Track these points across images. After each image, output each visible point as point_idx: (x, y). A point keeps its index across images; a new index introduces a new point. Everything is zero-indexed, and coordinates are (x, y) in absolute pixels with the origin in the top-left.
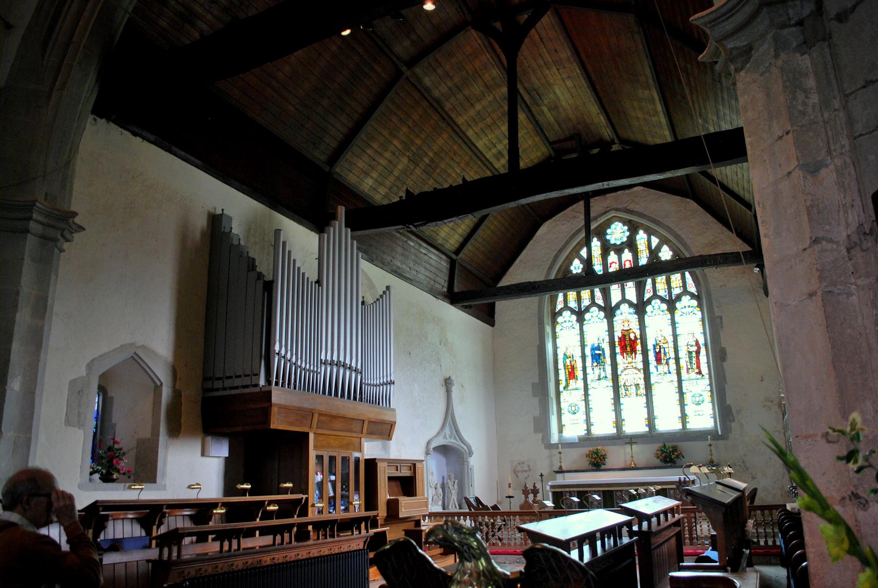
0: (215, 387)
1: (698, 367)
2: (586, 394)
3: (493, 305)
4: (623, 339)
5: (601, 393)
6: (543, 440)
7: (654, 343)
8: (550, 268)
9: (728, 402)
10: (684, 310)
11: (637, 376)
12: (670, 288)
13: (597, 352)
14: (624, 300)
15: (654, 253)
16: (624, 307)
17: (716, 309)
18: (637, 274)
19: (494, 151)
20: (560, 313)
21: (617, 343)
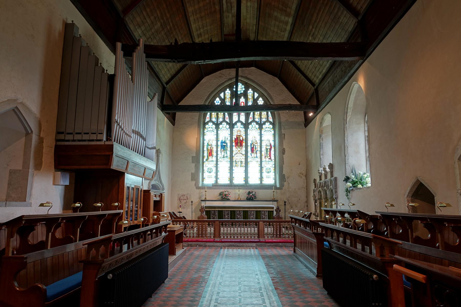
0: (67, 138)
1: (270, 156)
2: (217, 164)
3: (175, 113)
4: (237, 139)
5: (224, 165)
6: (195, 185)
7: (251, 143)
8: (206, 100)
9: (284, 173)
10: (266, 129)
11: (241, 157)
12: (261, 118)
13: (224, 144)
14: (239, 121)
15: (255, 101)
16: (239, 124)
17: (283, 130)
18: (247, 109)
19: (199, 32)
20: (207, 123)
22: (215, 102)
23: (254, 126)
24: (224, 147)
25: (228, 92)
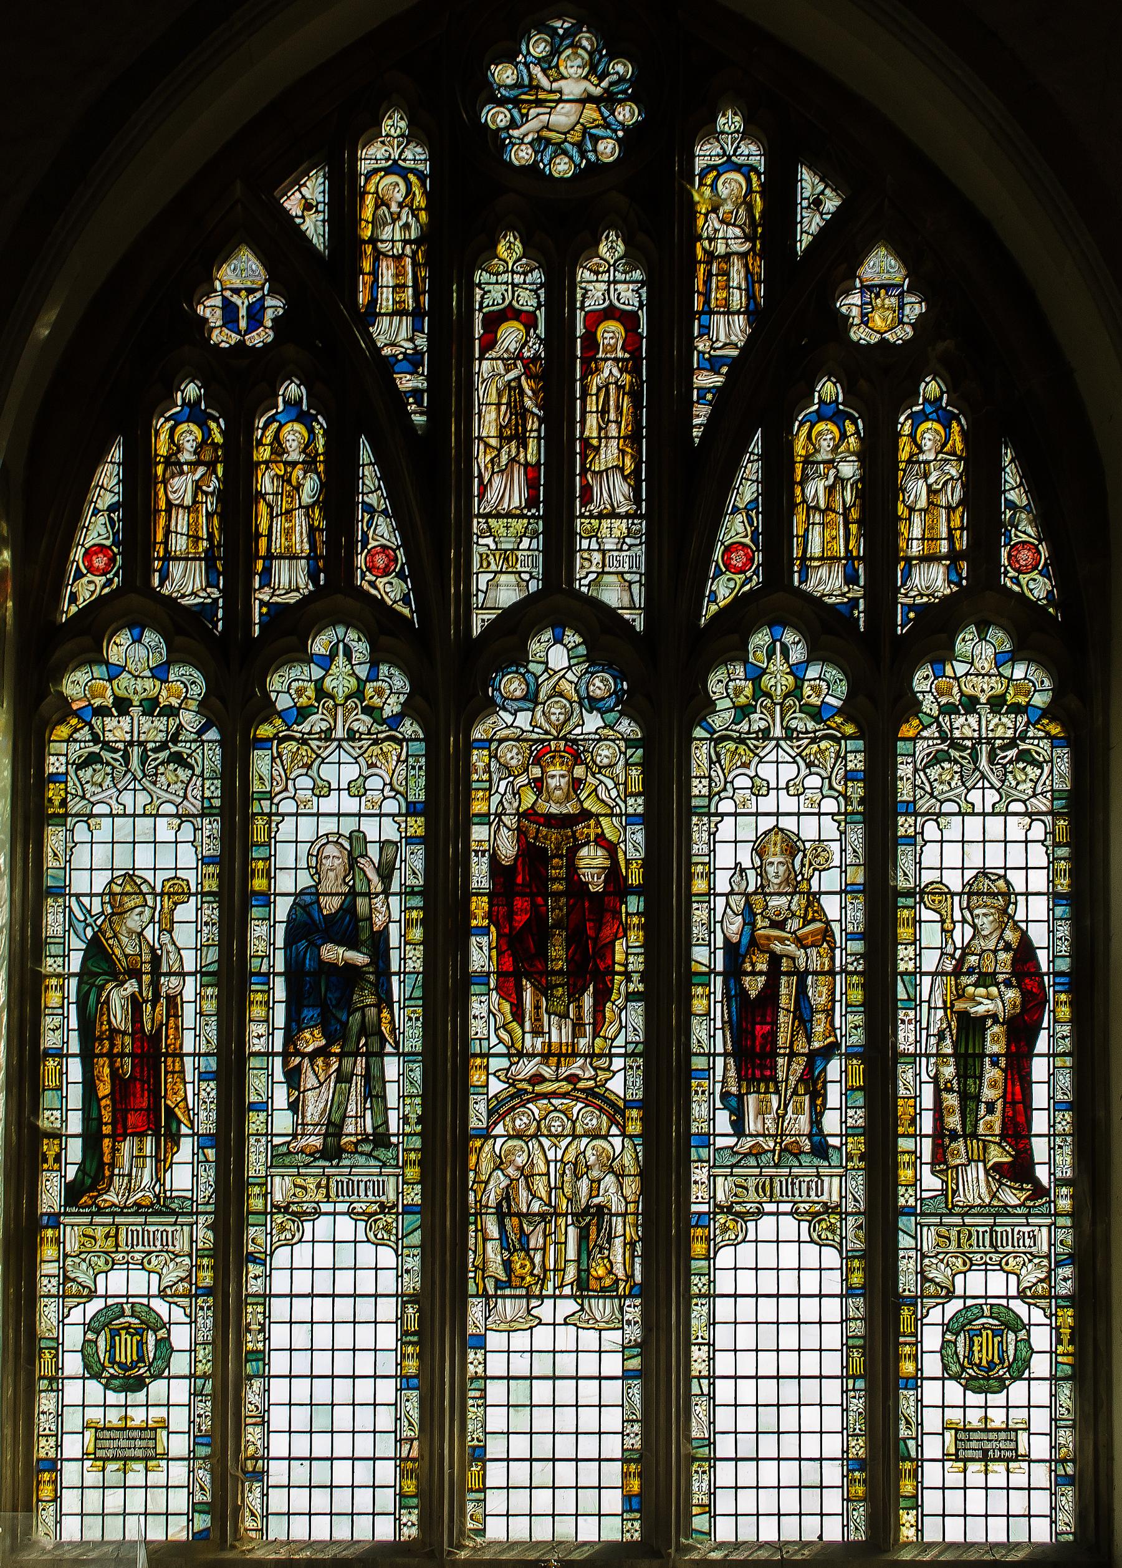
1: (1017, 1131)
10: (965, 726)
13: (334, 953)
14: (557, 602)
16: (556, 655)
21: (479, 906)
22: (210, 310)
23: (778, 680)
24: (332, 1000)
25: (392, 160)
